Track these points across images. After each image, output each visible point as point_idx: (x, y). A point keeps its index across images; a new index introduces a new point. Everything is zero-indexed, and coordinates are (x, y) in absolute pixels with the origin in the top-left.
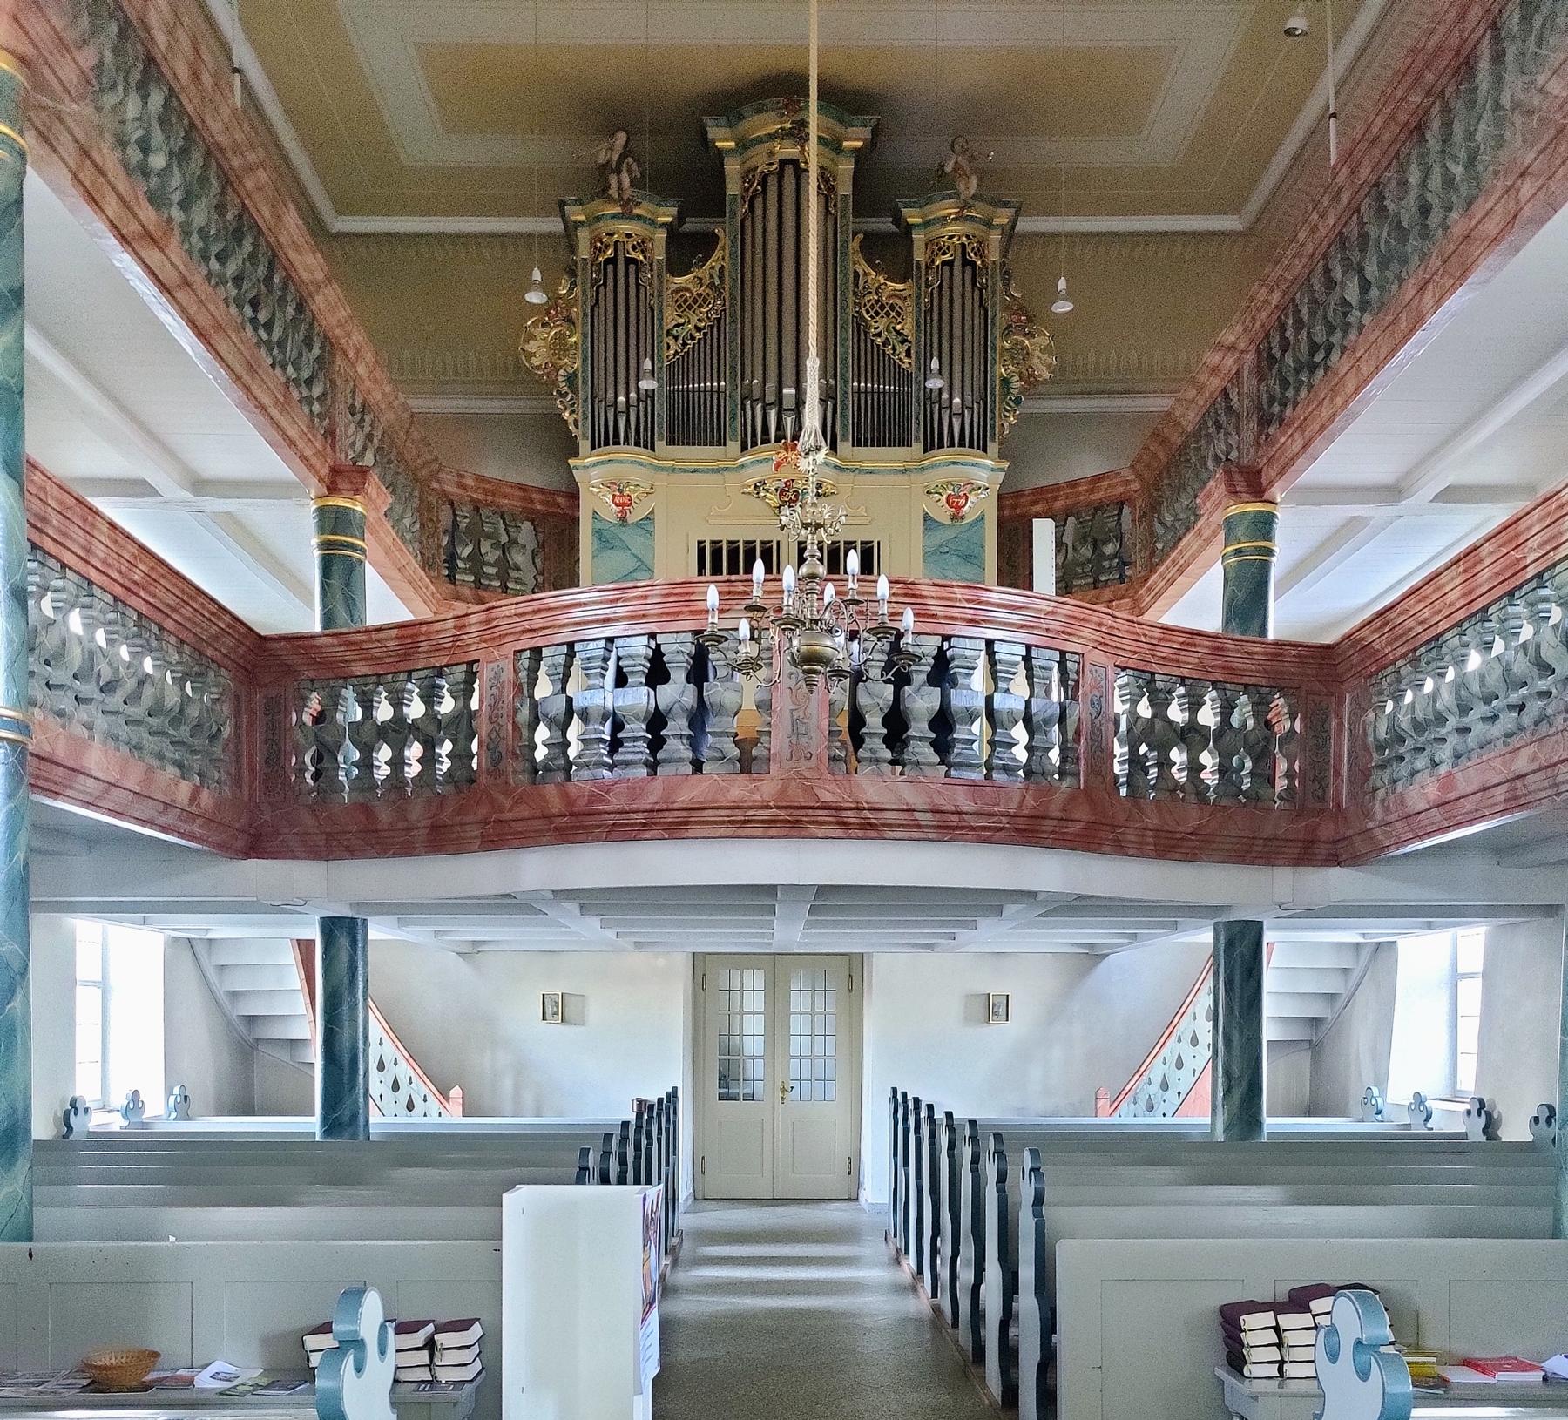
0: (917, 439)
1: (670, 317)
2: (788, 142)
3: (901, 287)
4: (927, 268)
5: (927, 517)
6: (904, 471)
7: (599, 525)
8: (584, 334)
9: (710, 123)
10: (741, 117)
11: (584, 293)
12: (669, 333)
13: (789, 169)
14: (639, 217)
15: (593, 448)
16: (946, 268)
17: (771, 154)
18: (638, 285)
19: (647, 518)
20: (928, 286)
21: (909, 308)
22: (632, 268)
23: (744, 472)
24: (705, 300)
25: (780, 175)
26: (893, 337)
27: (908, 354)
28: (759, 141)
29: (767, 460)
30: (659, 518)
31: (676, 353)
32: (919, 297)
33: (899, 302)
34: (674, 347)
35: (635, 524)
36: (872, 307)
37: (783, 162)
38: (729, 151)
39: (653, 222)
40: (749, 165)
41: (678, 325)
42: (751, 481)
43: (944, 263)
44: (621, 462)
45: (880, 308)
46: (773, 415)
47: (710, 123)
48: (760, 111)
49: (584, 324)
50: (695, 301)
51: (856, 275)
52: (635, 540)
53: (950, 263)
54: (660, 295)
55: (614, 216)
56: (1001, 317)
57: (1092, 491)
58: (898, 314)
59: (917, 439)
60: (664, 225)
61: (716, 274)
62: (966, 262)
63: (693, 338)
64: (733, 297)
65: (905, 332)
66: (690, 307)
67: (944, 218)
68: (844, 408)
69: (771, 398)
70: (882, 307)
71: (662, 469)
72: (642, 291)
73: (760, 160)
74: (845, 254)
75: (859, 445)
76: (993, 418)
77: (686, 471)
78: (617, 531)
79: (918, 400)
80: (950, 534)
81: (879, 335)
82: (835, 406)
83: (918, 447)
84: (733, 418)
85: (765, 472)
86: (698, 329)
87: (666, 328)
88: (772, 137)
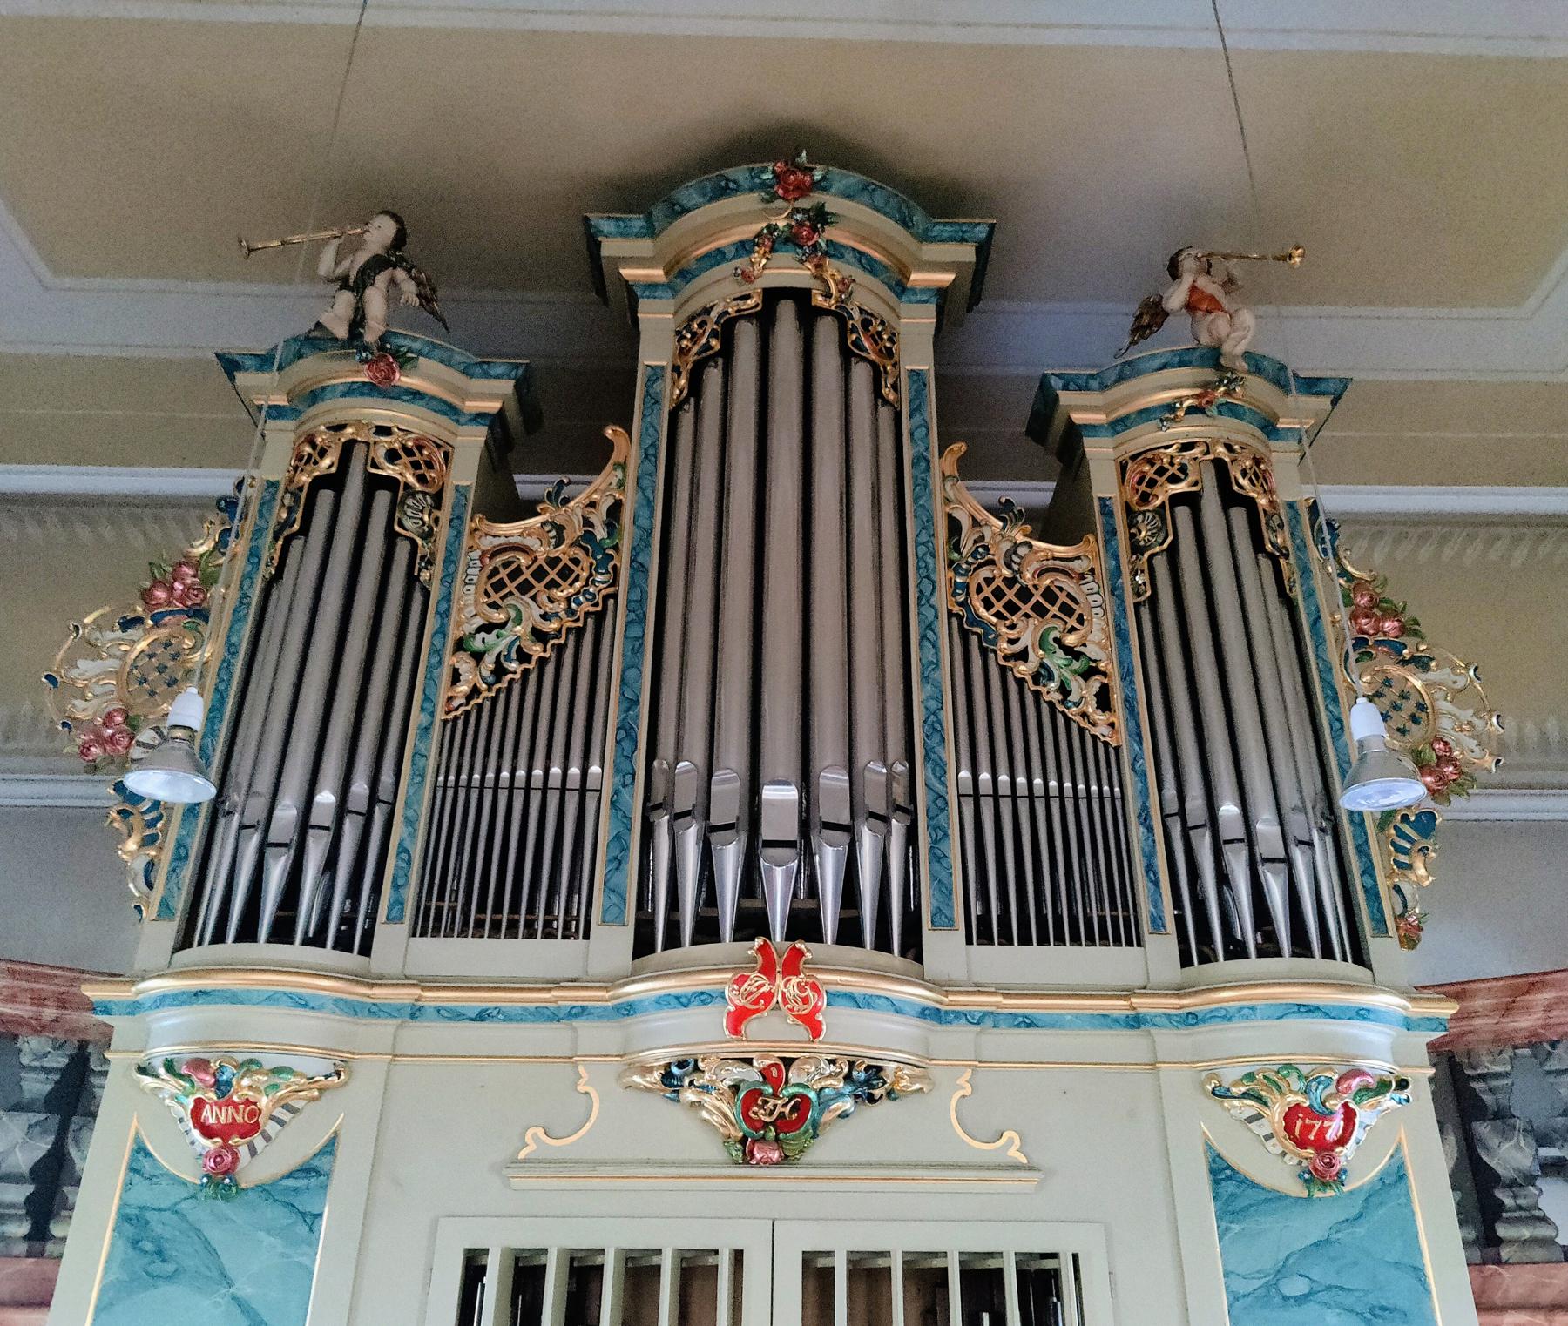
0: (1157, 924)
1: (469, 608)
2: (786, 257)
3: (1061, 550)
4: (1130, 512)
5: (1221, 1171)
6: (1136, 1022)
7: (144, 1194)
8: (231, 648)
9: (607, 226)
10: (678, 211)
11: (254, 554)
12: (460, 645)
13: (786, 310)
14: (416, 395)
15: (185, 940)
16: (1183, 513)
17: (747, 277)
18: (391, 538)
19: (307, 1170)
20: (1136, 549)
21: (1092, 598)
22: (382, 498)
23: (635, 1023)
24: (565, 573)
25: (765, 320)
26: (1057, 661)
27: (1103, 701)
28: (718, 256)
29: (703, 998)
30: (348, 1170)
31: (476, 690)
32: (1117, 573)
33: (1069, 585)
34: (469, 677)
35: (266, 1190)
36: (998, 594)
37: (773, 296)
38: (652, 286)
39: (451, 410)
40: (695, 306)
41: (488, 628)
42: (661, 1055)
43: (1176, 500)
44: (232, 998)
45: (1016, 599)
46: (730, 859)
47: (607, 226)
48: (723, 191)
49: (237, 618)
50: (539, 574)
51: (954, 526)
52: (247, 1246)
53: (1191, 500)
54: (451, 559)
55: (351, 390)
56: (1336, 622)
57: (1508, 1009)
58: (1067, 610)
59: (1157, 924)
60: (478, 417)
61: (599, 518)
62: (1230, 498)
63: (523, 657)
64: (639, 568)
65: (1092, 651)
66: (525, 588)
67: (1170, 408)
68: (940, 834)
69: (728, 805)
70: (1025, 594)
71: (375, 1011)
72: (402, 550)
73: (720, 292)
74: (923, 484)
75: (985, 938)
76: (1368, 871)
77: (457, 1016)
78: (202, 1213)
79: (1145, 819)
80: (1308, 1228)
81: (1023, 656)
82: (911, 837)
83: (1161, 949)
84: (618, 862)
85: (701, 1030)
86: (539, 636)
87: (453, 634)
88: (744, 247)
